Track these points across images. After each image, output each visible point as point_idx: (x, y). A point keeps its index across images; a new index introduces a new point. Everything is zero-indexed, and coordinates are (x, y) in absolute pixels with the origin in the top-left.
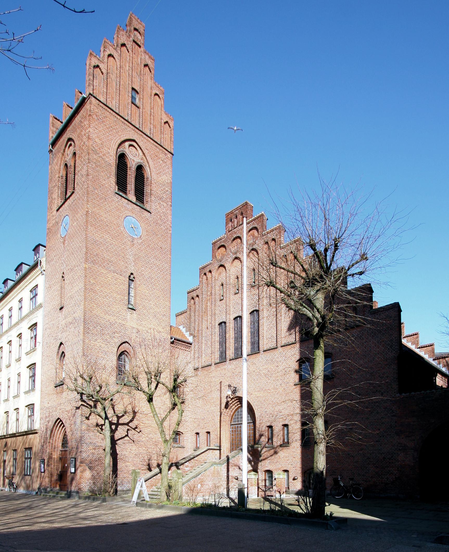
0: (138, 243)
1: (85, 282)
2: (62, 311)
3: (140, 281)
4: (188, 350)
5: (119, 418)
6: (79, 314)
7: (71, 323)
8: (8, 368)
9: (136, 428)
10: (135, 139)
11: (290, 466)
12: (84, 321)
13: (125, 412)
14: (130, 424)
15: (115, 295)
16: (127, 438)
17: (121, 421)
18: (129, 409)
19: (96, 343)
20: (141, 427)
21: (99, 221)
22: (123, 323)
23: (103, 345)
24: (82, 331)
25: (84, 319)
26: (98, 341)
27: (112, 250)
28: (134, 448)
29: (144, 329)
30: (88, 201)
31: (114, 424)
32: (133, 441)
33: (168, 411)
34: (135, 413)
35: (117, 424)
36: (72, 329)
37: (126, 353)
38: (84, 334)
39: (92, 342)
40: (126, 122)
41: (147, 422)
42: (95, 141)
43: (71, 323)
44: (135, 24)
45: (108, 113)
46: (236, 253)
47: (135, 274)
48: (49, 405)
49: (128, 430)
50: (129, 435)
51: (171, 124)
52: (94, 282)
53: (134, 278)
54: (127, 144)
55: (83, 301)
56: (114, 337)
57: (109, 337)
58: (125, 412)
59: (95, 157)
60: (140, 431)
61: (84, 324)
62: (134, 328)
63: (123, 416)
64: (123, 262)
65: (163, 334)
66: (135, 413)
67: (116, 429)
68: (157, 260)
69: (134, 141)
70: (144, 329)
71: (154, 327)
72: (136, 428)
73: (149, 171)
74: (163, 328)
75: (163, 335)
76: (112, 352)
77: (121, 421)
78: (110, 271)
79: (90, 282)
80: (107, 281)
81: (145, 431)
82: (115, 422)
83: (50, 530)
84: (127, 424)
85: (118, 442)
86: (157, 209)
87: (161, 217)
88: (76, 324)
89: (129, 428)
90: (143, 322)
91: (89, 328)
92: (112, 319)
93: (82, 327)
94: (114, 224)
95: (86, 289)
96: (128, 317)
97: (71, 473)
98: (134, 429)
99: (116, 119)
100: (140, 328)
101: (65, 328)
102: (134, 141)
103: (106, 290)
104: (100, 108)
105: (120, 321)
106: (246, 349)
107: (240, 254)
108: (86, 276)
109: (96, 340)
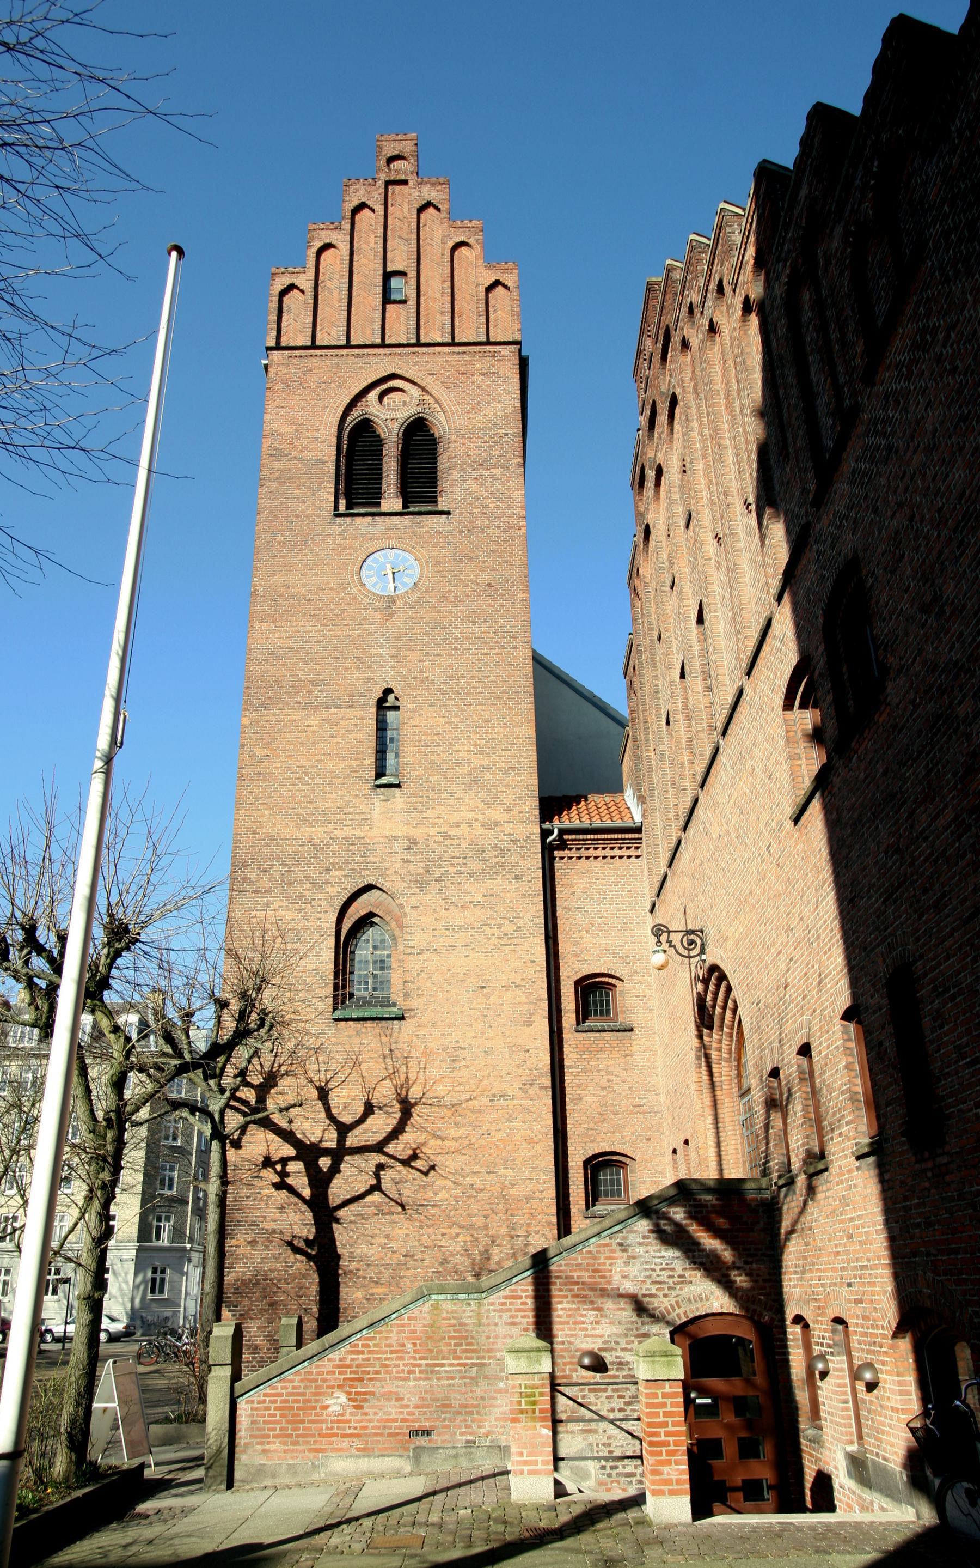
4: (632, 852)
5: (344, 1130)
9: (415, 1157)
10: (393, 371)
13: (369, 1109)
14: (390, 1148)
15: (330, 764)
16: (376, 1197)
17: (352, 1140)
18: (385, 1093)
20: (431, 1149)
22: (359, 833)
28: (399, 1232)
29: (433, 831)
31: (327, 1152)
32: (402, 1206)
34: (407, 1108)
35: (338, 1154)
37: (376, 920)
41: (453, 1132)
44: (390, 149)
45: (314, 360)
47: (398, 690)
49: (380, 1167)
50: (384, 1187)
51: (510, 279)
52: (266, 752)
53: (396, 698)
54: (373, 395)
56: (327, 882)
57: (308, 886)
58: (369, 1109)
59: (277, 466)
60: (433, 1168)
62: (396, 838)
63: (361, 1120)
65: (508, 828)
66: (407, 1108)
67: (335, 1169)
68: (474, 623)
69: (393, 376)
70: (433, 831)
71: (471, 815)
72: (415, 1157)
74: (508, 810)
75: (508, 831)
77: (352, 1140)
80: (307, 737)
81: (447, 1164)
82: (333, 1145)
84: (378, 1148)
85: (341, 1213)
89: (383, 1159)
90: (429, 813)
92: (319, 833)
96: (376, 814)
98: (406, 1163)
100: (418, 833)
102: (393, 376)
104: (426, 358)
105: (348, 832)
106: (637, 836)
109: (267, 905)
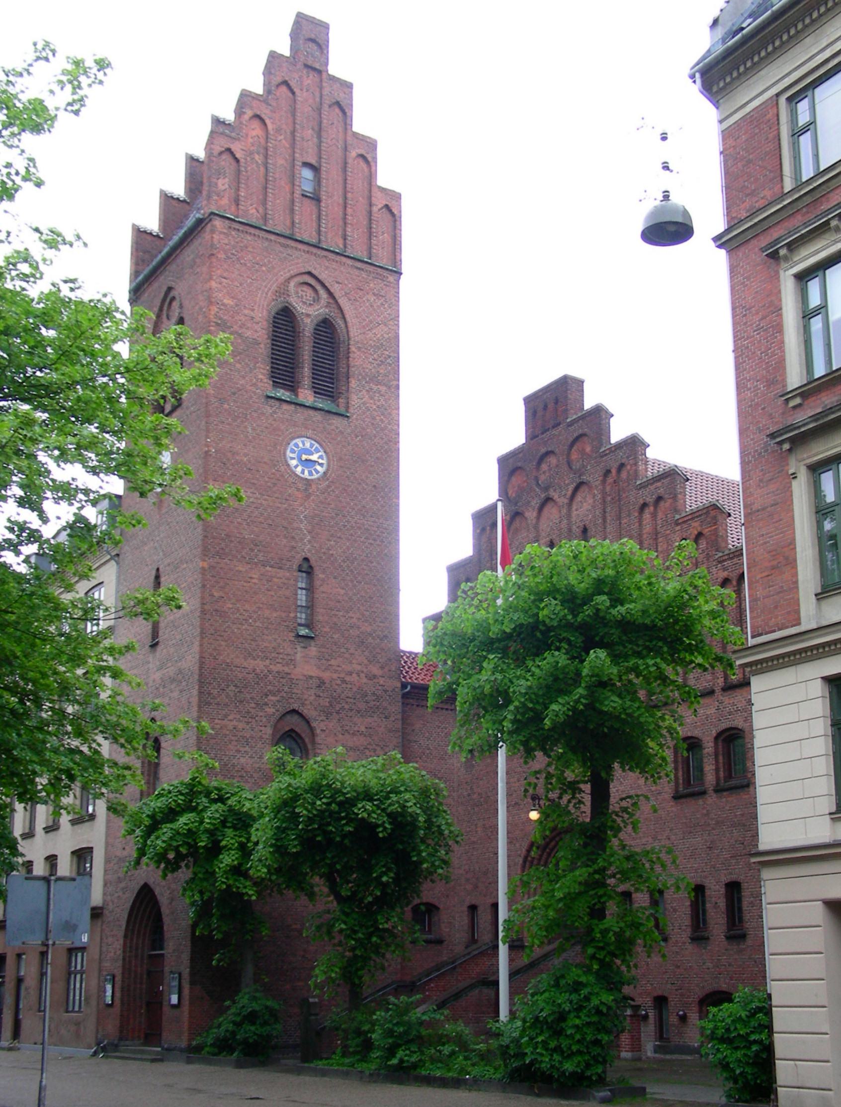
0: (318, 489)
1: (203, 598)
2: (155, 651)
3: (324, 572)
6: (190, 661)
7: (173, 680)
8: (51, 835)
11: (669, 986)
12: (200, 681)
19: (225, 722)
21: (232, 465)
22: (286, 669)
23: (240, 726)
24: (195, 700)
25: (200, 675)
26: (230, 717)
27: (261, 519)
29: (335, 676)
30: (208, 431)
33: (601, 478)
36: (176, 694)
38: (200, 707)
39: (216, 721)
40: (289, 242)
42: (223, 305)
43: (173, 680)
46: (546, 489)
48: (125, 853)
55: (198, 639)
61: (200, 687)
62: (311, 677)
64: (286, 537)
68: (364, 517)
70: (335, 676)
71: (359, 668)
73: (343, 326)
75: (382, 682)
76: (261, 738)
78: (256, 564)
79: (212, 595)
83: (164, 210)
86: (364, 403)
87: (374, 419)
88: (184, 683)
90: (333, 662)
91: (209, 694)
93: (195, 692)
94: (265, 463)
95: (203, 612)
97: (174, 1006)
99: (266, 244)
100: (326, 675)
101: (161, 690)
103: (247, 607)
105: (279, 667)
107: (555, 490)
108: (204, 586)
109: (226, 716)
